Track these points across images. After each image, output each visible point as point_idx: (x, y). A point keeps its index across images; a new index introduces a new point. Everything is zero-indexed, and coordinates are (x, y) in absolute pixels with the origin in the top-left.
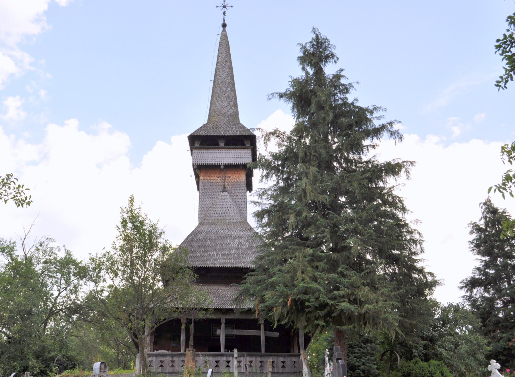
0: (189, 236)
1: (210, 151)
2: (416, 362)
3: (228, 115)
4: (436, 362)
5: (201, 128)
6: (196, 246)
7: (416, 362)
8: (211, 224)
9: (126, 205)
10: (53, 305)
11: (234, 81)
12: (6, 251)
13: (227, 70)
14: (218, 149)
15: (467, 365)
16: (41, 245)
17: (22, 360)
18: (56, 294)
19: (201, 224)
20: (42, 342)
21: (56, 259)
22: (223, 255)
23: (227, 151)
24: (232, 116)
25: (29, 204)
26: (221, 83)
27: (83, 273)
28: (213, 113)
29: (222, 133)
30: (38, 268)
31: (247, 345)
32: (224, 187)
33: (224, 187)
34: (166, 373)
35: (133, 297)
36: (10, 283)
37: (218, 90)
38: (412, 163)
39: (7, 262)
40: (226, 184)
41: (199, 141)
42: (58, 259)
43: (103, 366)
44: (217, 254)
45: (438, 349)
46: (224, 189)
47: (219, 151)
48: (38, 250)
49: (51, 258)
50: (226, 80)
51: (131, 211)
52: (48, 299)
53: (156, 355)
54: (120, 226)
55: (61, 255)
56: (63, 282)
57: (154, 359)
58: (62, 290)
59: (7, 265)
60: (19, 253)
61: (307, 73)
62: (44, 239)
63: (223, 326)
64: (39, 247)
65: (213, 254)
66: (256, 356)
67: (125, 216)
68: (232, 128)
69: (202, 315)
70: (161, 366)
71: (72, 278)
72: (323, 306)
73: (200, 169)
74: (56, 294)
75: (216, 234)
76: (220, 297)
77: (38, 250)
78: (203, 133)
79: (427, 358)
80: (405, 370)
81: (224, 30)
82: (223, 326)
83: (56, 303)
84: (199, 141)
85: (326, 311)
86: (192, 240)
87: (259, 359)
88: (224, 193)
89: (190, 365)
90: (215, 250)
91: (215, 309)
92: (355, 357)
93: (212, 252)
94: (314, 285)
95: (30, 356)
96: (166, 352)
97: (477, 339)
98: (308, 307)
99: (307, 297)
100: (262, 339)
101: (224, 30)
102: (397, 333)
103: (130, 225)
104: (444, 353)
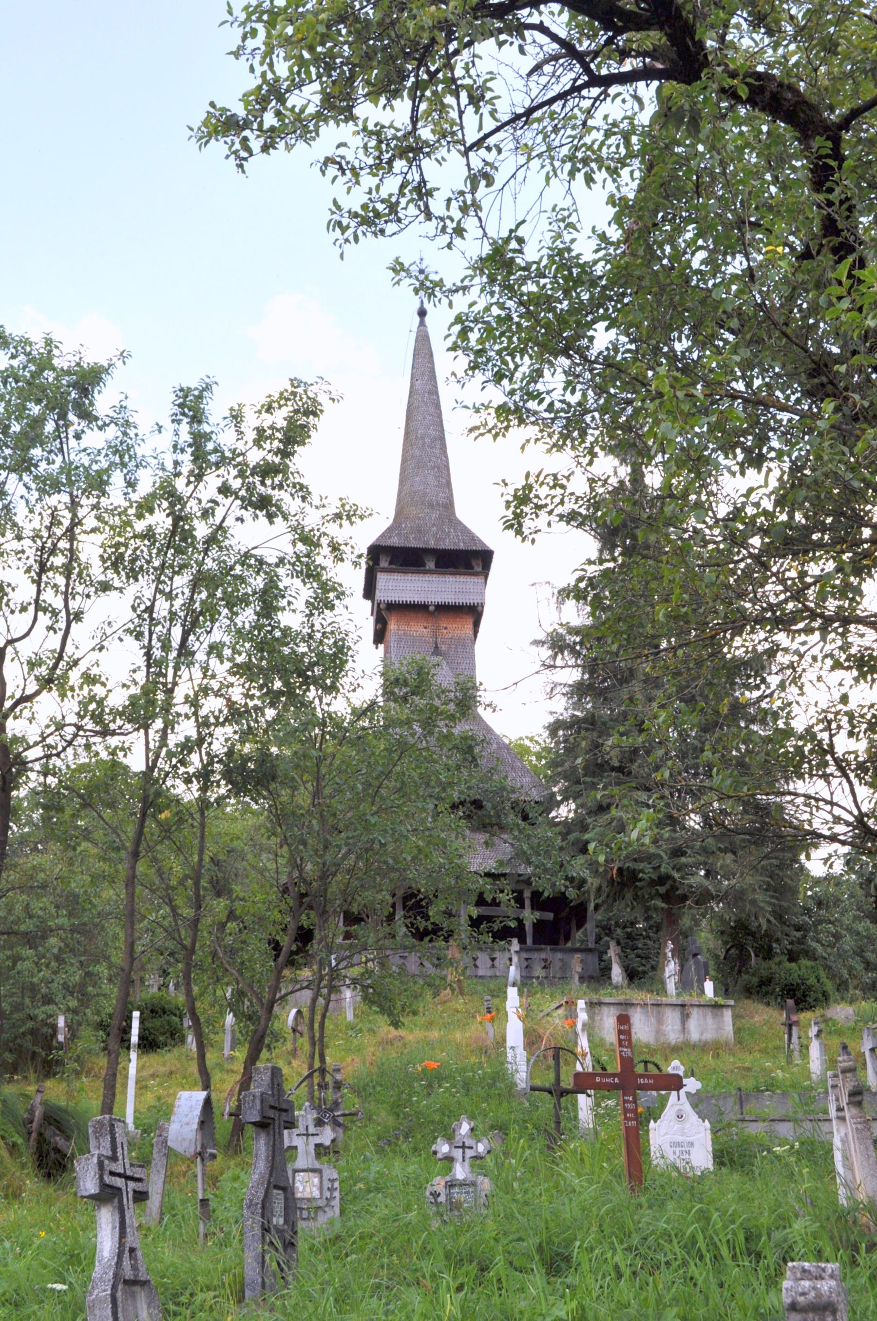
1: (409, 577)
2: (780, 963)
4: (809, 963)
7: (780, 963)
15: (851, 969)
23: (441, 578)
26: (422, 438)
29: (432, 544)
37: (417, 452)
45: (810, 942)
47: (427, 577)
68: (448, 534)
72: (663, 879)
79: (792, 957)
80: (764, 973)
81: (422, 323)
85: (668, 886)
92: (638, 956)
97: (868, 929)
98: (641, 880)
101: (422, 323)
102: (769, 921)
104: (820, 949)
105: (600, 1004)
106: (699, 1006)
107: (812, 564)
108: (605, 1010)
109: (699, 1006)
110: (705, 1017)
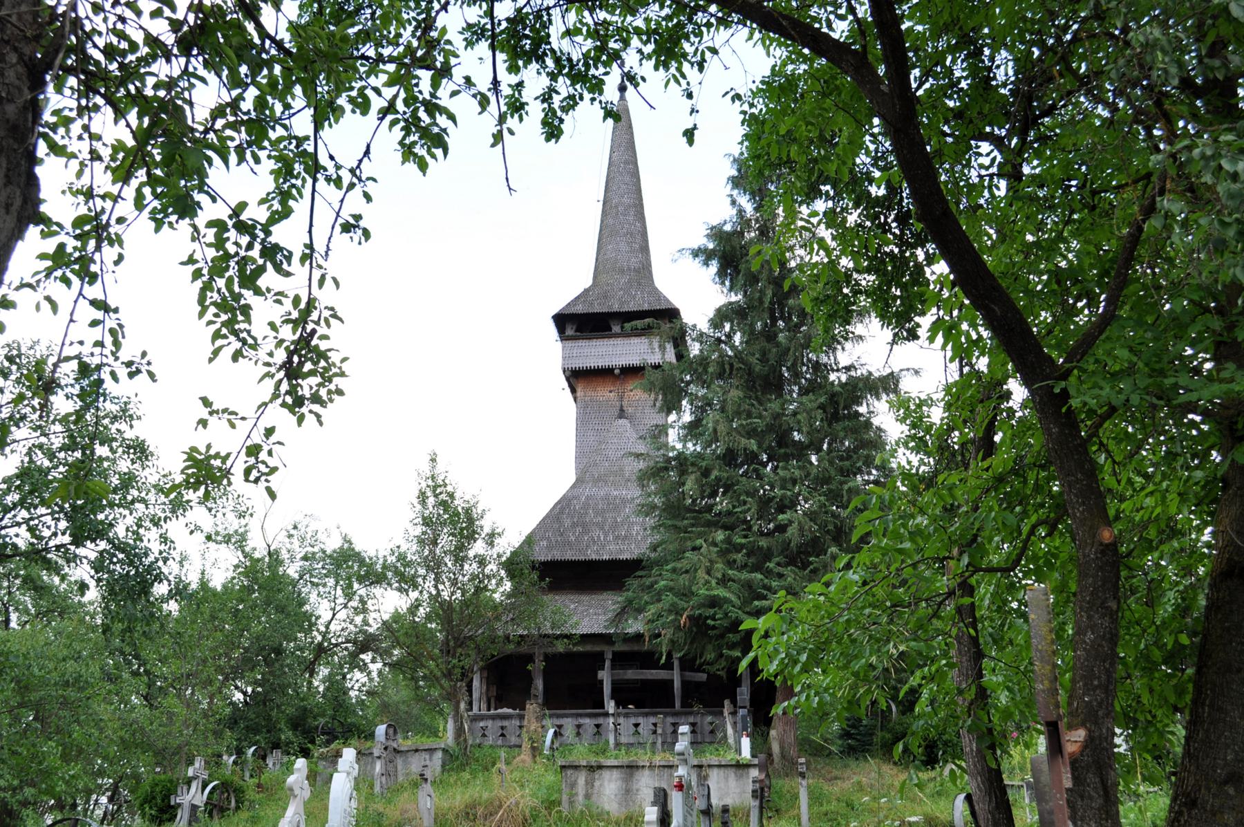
0: (556, 504)
1: (594, 342)
3: (629, 269)
5: (577, 298)
6: (567, 522)
8: (599, 480)
9: (426, 469)
10: (324, 637)
11: (641, 199)
12: (233, 540)
13: (627, 179)
14: (610, 337)
16: (295, 527)
17: (269, 731)
18: (326, 615)
19: (579, 481)
20: (302, 700)
21: (324, 552)
22: (617, 538)
24: (637, 271)
25: (251, 515)
27: (373, 575)
28: (601, 268)
29: (616, 308)
30: (292, 571)
31: (645, 697)
32: (622, 410)
33: (622, 410)
34: (510, 747)
35: (459, 620)
36: (242, 601)
38: (917, 372)
39: (236, 562)
40: (625, 403)
41: (575, 324)
42: (328, 552)
43: (391, 731)
44: (606, 536)
46: (622, 414)
47: (612, 341)
48: (290, 536)
49: (316, 549)
50: (626, 200)
51: (433, 478)
52: (311, 625)
53: (493, 718)
54: (415, 501)
55: (333, 544)
56: (339, 592)
57: (489, 723)
58: (338, 608)
59: (236, 567)
60: (257, 545)
61: (741, 212)
62: (298, 518)
63: (607, 664)
64: (292, 532)
65: (599, 537)
66: (666, 715)
67: (424, 485)
69: (560, 647)
70: (503, 735)
71: (356, 586)
73: (577, 377)
74: (326, 615)
75: (606, 498)
76: (588, 615)
77: (290, 536)
78: (580, 309)
82: (607, 664)
83: (327, 632)
84: (575, 324)
86: (562, 511)
87: (670, 720)
88: (621, 421)
89: (533, 728)
90: (602, 528)
91: (583, 636)
93: (597, 533)
94: (721, 592)
95: (283, 726)
96: (510, 711)
98: (714, 628)
99: (712, 611)
100: (677, 684)
103: (431, 501)
105: (600, 767)
106: (720, 766)
107: (269, 184)
108: (606, 774)
109: (720, 766)
110: (726, 779)
